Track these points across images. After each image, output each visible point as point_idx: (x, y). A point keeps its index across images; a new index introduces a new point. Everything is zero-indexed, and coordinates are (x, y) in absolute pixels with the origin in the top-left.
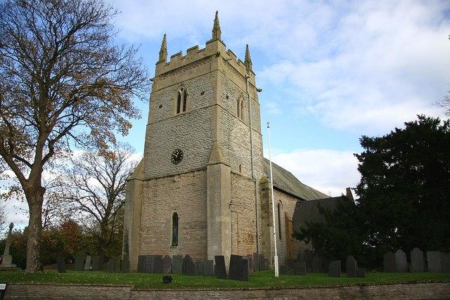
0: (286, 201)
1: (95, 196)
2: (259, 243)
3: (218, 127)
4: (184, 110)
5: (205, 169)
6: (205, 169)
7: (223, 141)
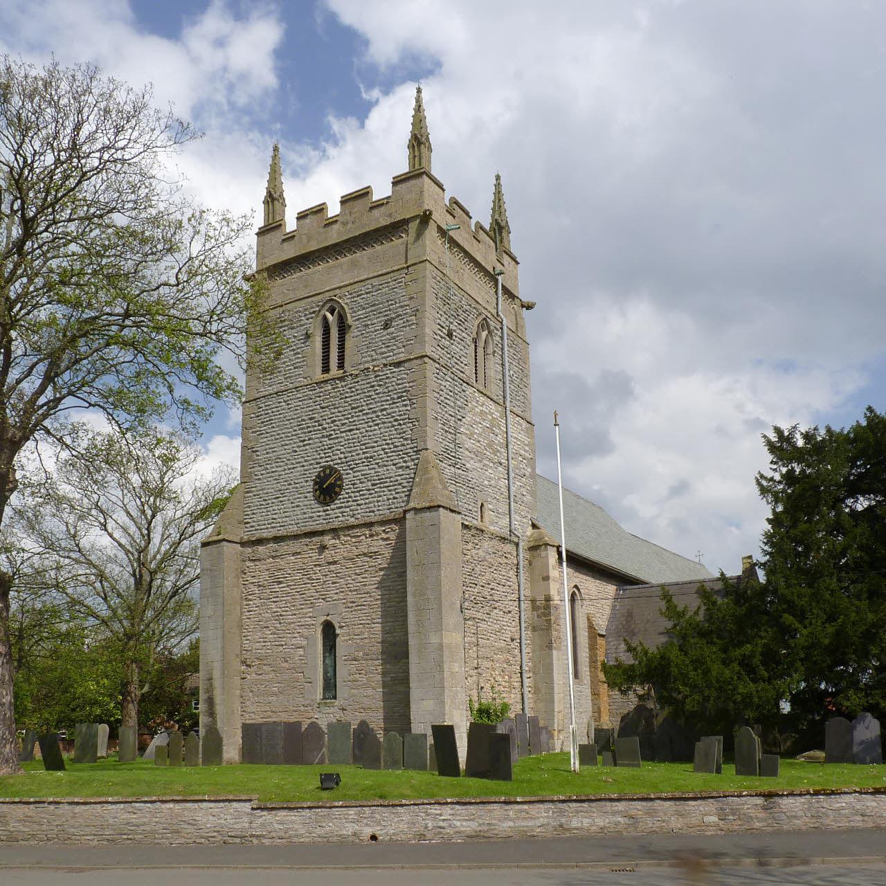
0: (600, 594)
1: (101, 576)
2: (526, 690)
3: (430, 414)
4: (341, 366)
5: (400, 521)
6: (400, 521)
7: (439, 450)
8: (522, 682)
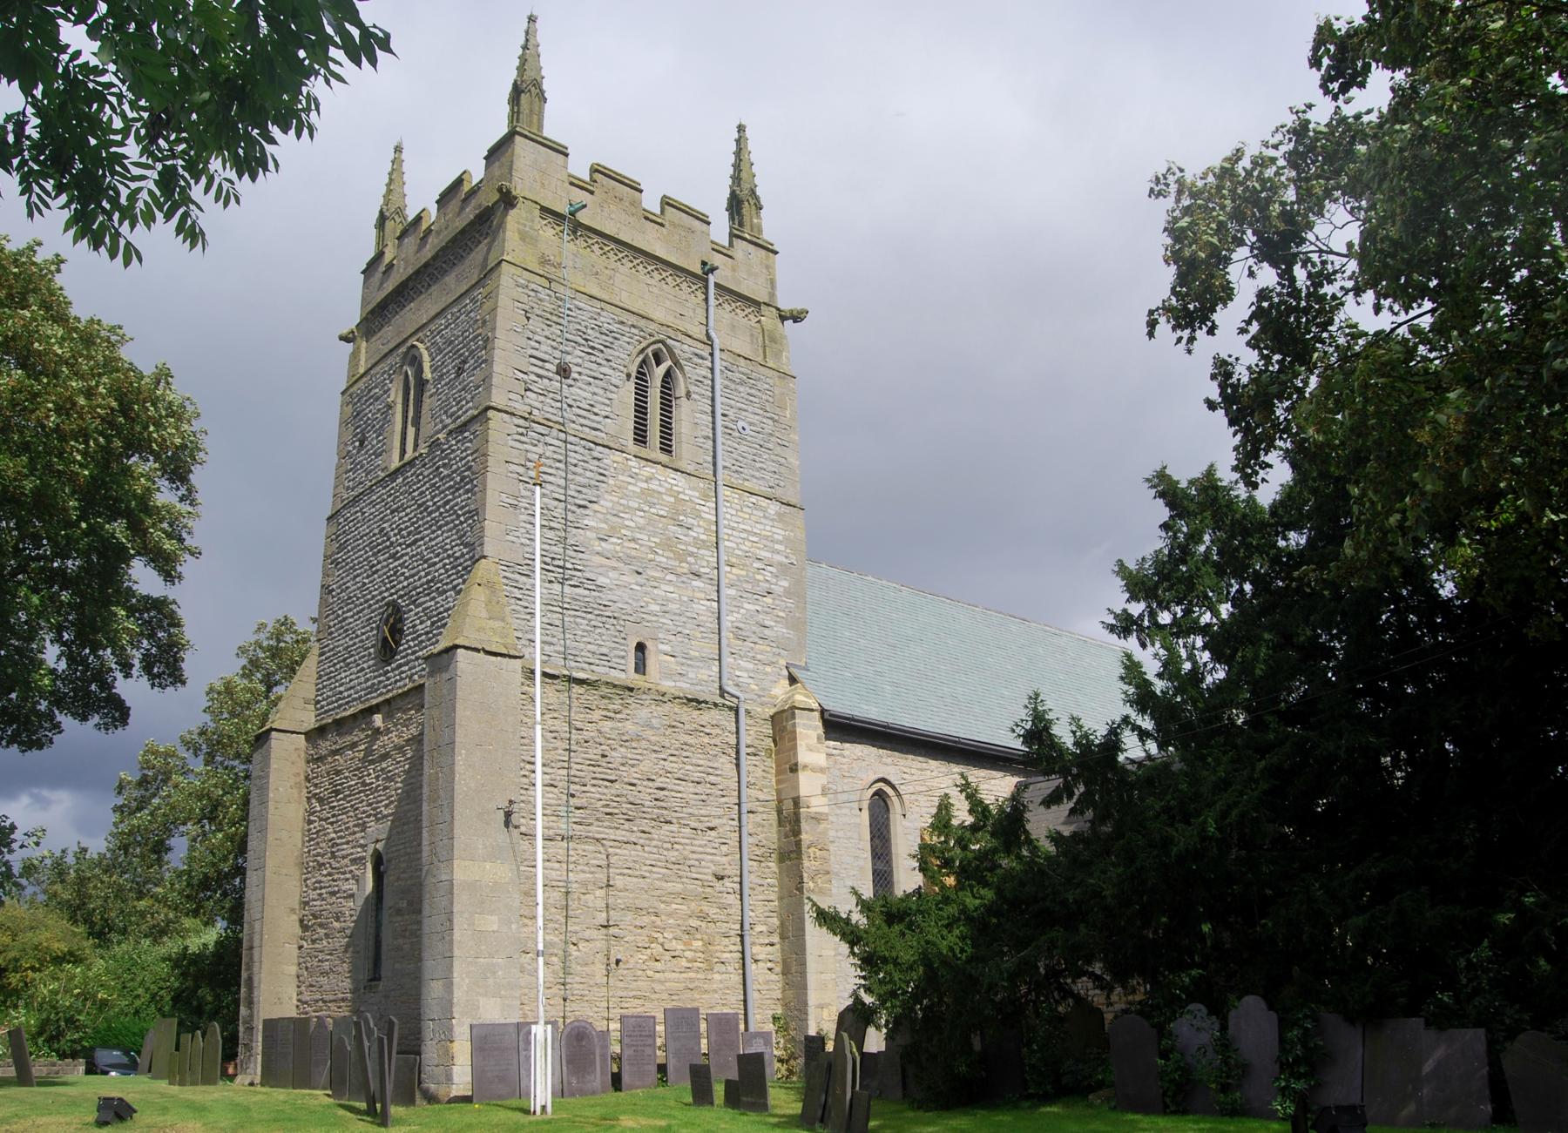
8: (743, 953)
